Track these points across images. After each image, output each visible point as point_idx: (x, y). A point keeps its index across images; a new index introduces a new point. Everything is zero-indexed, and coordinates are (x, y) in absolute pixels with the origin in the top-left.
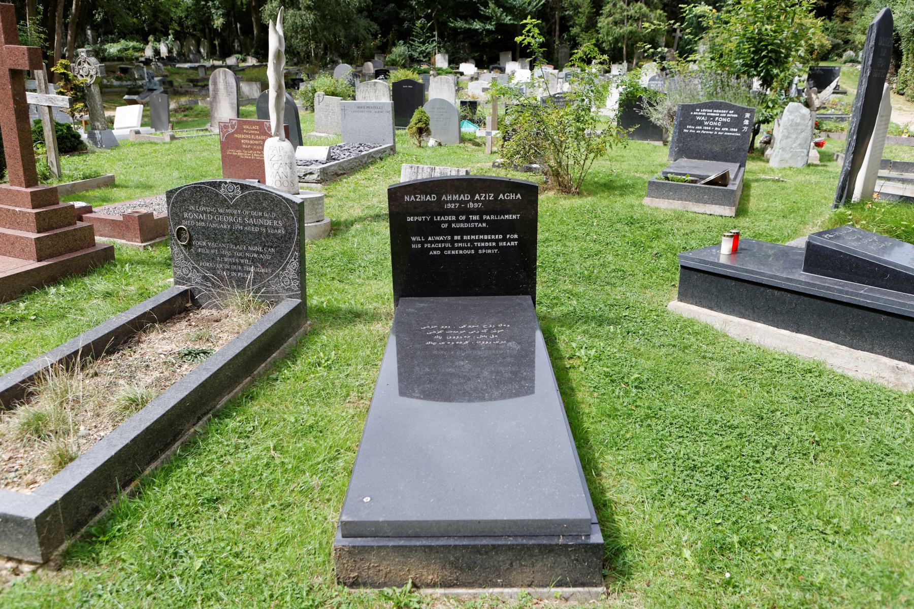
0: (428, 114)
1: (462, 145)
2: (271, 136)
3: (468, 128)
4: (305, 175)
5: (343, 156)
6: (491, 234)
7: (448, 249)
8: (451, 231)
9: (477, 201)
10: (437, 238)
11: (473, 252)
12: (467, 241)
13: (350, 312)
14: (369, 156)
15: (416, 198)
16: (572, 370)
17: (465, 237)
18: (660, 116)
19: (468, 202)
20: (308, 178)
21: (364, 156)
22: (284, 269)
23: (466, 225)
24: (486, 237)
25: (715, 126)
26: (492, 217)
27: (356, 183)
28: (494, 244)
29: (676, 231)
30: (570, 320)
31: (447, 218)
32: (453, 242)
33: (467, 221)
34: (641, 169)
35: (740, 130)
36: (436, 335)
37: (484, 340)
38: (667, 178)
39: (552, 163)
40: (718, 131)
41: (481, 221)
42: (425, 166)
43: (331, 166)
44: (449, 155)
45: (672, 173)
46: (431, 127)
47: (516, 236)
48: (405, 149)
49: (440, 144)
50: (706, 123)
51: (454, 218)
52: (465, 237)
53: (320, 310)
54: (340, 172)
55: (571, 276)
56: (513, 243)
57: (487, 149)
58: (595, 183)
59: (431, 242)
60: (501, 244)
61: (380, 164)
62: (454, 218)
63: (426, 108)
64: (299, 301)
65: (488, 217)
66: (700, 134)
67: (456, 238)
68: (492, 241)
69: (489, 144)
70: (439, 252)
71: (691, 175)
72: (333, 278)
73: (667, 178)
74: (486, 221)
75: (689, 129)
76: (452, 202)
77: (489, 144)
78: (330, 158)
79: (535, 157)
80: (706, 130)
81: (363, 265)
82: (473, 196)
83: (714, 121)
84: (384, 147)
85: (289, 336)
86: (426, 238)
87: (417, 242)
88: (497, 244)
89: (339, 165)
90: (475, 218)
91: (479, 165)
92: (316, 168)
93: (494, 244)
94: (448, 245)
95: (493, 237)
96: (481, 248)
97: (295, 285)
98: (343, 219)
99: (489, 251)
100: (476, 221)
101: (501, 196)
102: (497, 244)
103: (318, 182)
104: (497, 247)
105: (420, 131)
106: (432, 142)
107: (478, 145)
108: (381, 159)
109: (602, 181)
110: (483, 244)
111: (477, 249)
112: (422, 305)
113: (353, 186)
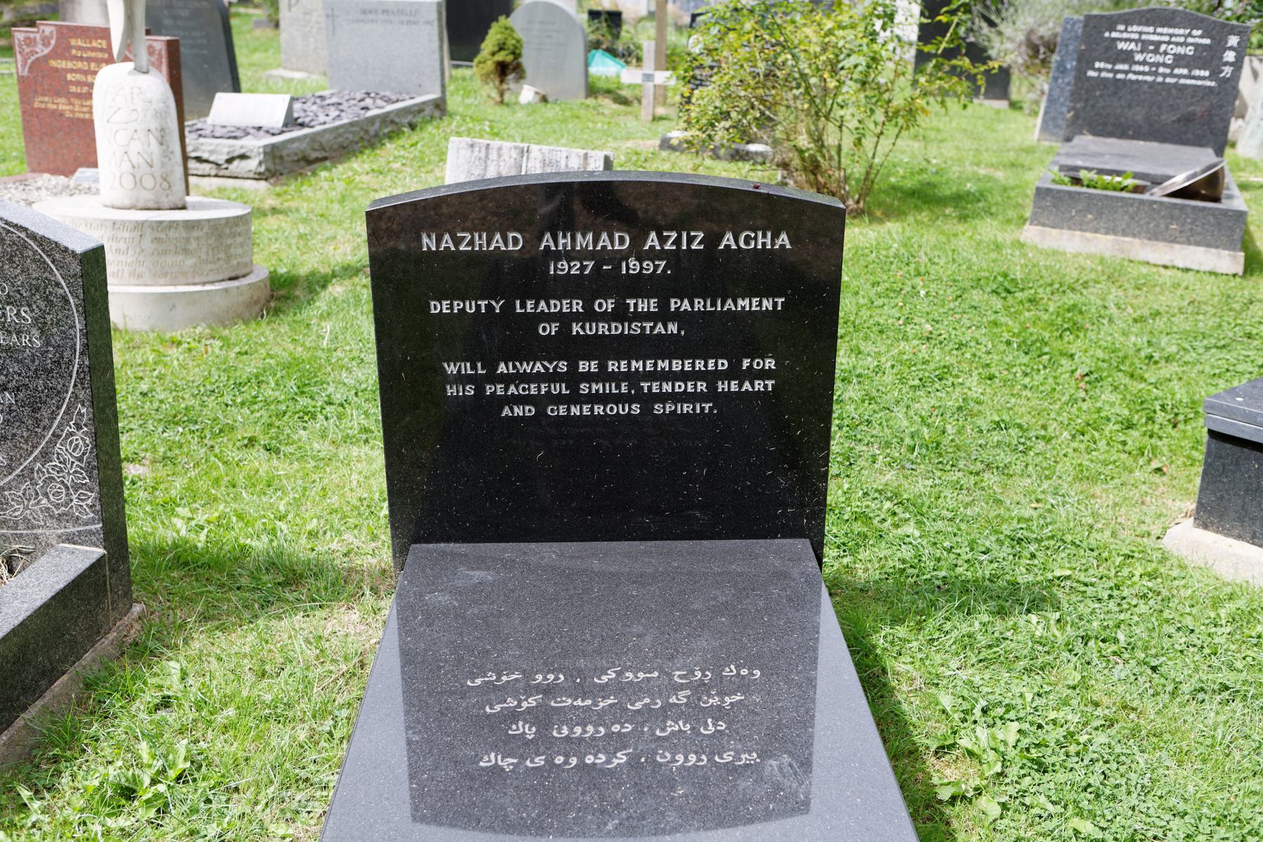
0: (520, 34)
1: (591, 101)
2: (110, 61)
3: (604, 67)
4: (230, 161)
5: (322, 118)
6: (694, 357)
7: (559, 400)
8: (568, 347)
9: (653, 255)
10: (526, 367)
11: (636, 409)
12: (617, 377)
13: (272, 565)
14: (385, 119)
15: (457, 242)
16: (959, 807)
17: (612, 366)
18: (1009, 46)
19: (625, 256)
20: (236, 166)
21: (372, 120)
22: (45, 456)
23: (616, 329)
24: (677, 366)
25: (1158, 65)
26: (699, 304)
27: (350, 181)
28: (702, 386)
29: (1113, 310)
30: (921, 595)
31: (555, 306)
32: (573, 378)
33: (620, 314)
34: (986, 157)
35: (1214, 75)
36: (513, 716)
37: (675, 742)
38: (1077, 181)
39: (803, 141)
40: (1165, 76)
41: (663, 315)
42: (507, 145)
43: (292, 141)
44: (564, 121)
45: (1089, 169)
46: (526, 61)
47: (770, 363)
48: (468, 106)
49: (544, 99)
50: (1139, 57)
51: (578, 306)
52: (612, 366)
53: (185, 561)
54: (314, 155)
55: (888, 444)
56: (759, 385)
57: (645, 111)
58: (894, 188)
59: (507, 380)
60: (722, 386)
61: (408, 138)
62: (578, 306)
63: (516, 21)
64: (100, 551)
65: (686, 305)
66: (1124, 82)
67: (583, 366)
68: (695, 376)
69: (648, 99)
70: (530, 411)
71: (1136, 176)
72: (252, 441)
73: (1077, 181)
74: (678, 316)
75: (1101, 69)
76: (569, 256)
77: (648, 99)
78: (291, 122)
79: (760, 127)
80: (1137, 74)
81: (338, 398)
82: (639, 240)
83: (1156, 52)
84: (419, 100)
85: (52, 675)
86: (491, 366)
87: (461, 379)
88: (712, 386)
89: (313, 138)
90: (643, 306)
91: (630, 144)
92: (255, 144)
93: (702, 386)
94: (560, 389)
95: (699, 365)
96: (663, 398)
97: (85, 504)
98: (303, 271)
99: (687, 408)
100: (647, 316)
101: (728, 240)
102: (712, 386)
103: (260, 177)
104: (712, 395)
105: (503, 70)
106: (527, 94)
107: (624, 102)
108: (412, 127)
109: (909, 184)
110: (667, 387)
111: (649, 400)
112: (478, 575)
113: (340, 186)
